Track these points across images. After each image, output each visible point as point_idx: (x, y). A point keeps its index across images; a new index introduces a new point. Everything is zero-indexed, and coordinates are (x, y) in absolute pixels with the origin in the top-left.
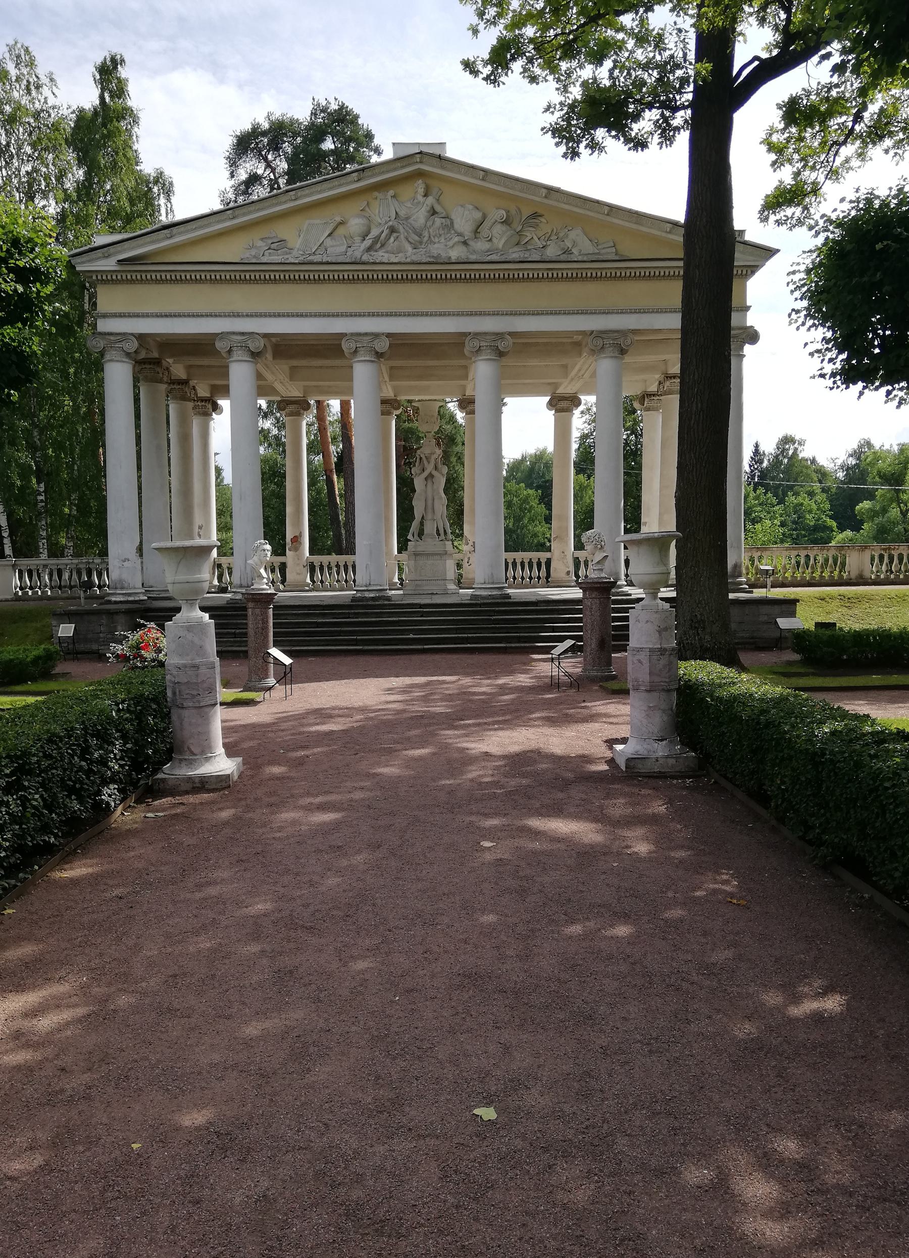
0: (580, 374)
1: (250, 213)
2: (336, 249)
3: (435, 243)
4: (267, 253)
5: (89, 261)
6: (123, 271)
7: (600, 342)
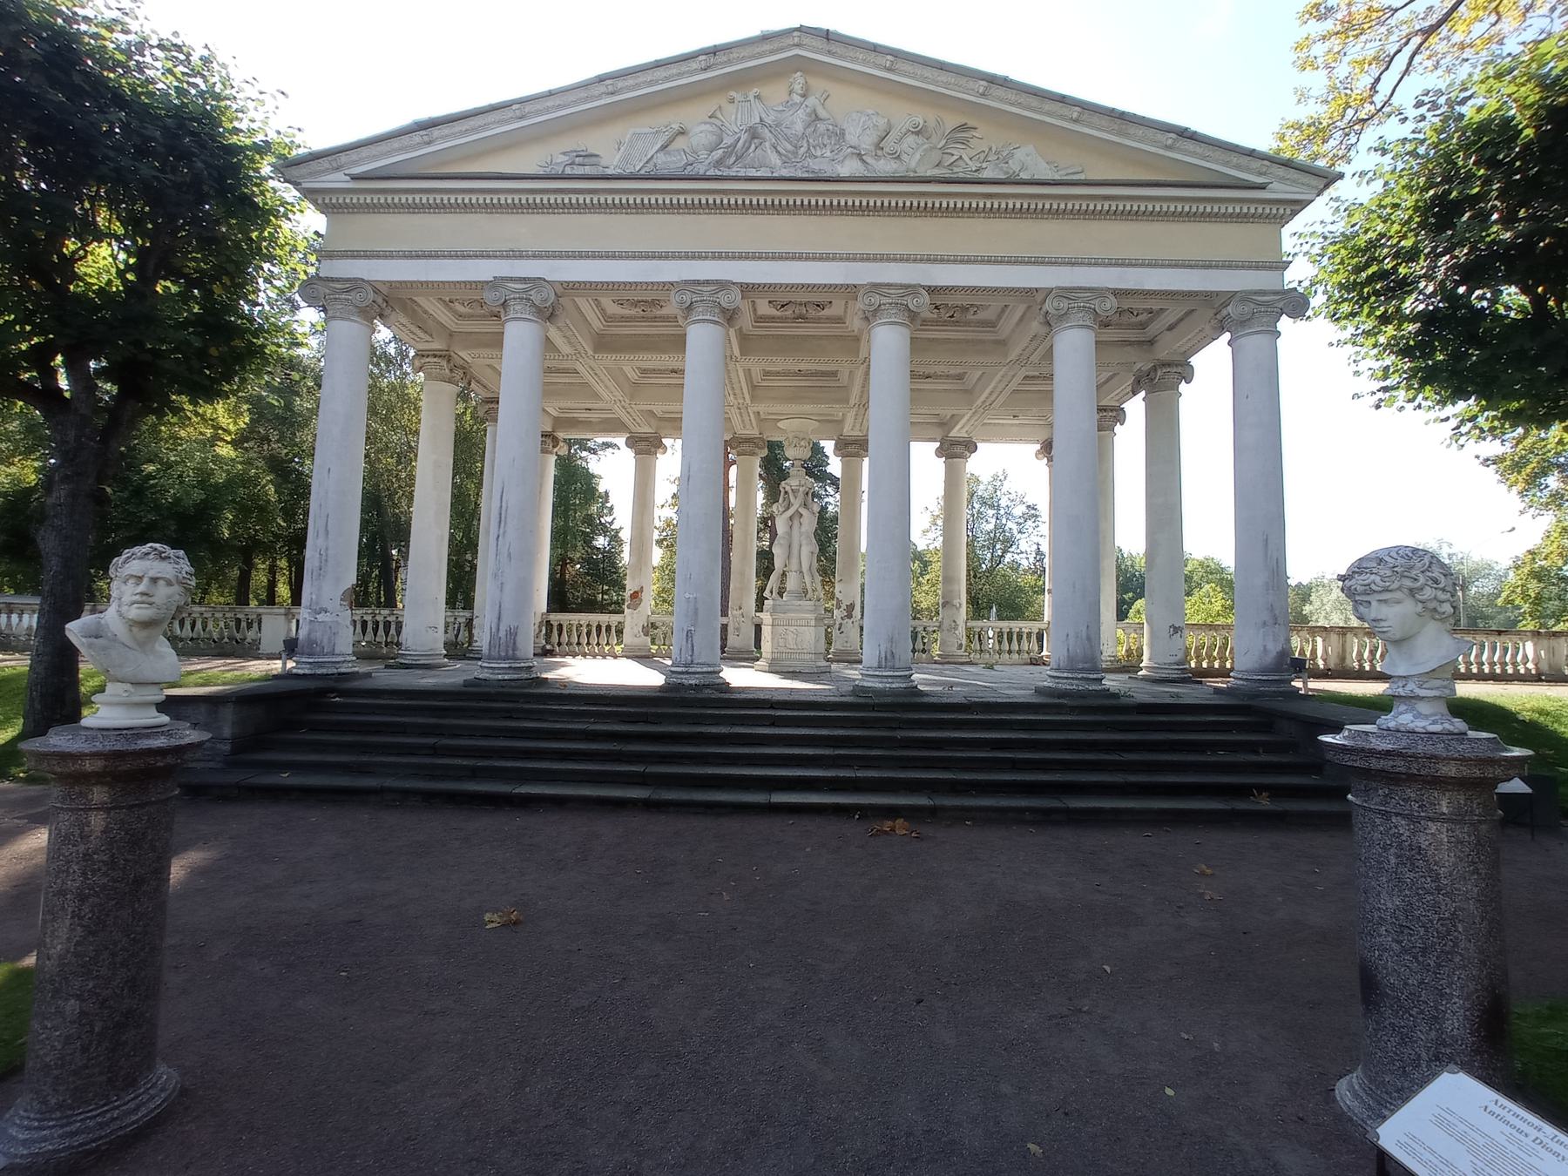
3: (816, 157)
5: (311, 174)
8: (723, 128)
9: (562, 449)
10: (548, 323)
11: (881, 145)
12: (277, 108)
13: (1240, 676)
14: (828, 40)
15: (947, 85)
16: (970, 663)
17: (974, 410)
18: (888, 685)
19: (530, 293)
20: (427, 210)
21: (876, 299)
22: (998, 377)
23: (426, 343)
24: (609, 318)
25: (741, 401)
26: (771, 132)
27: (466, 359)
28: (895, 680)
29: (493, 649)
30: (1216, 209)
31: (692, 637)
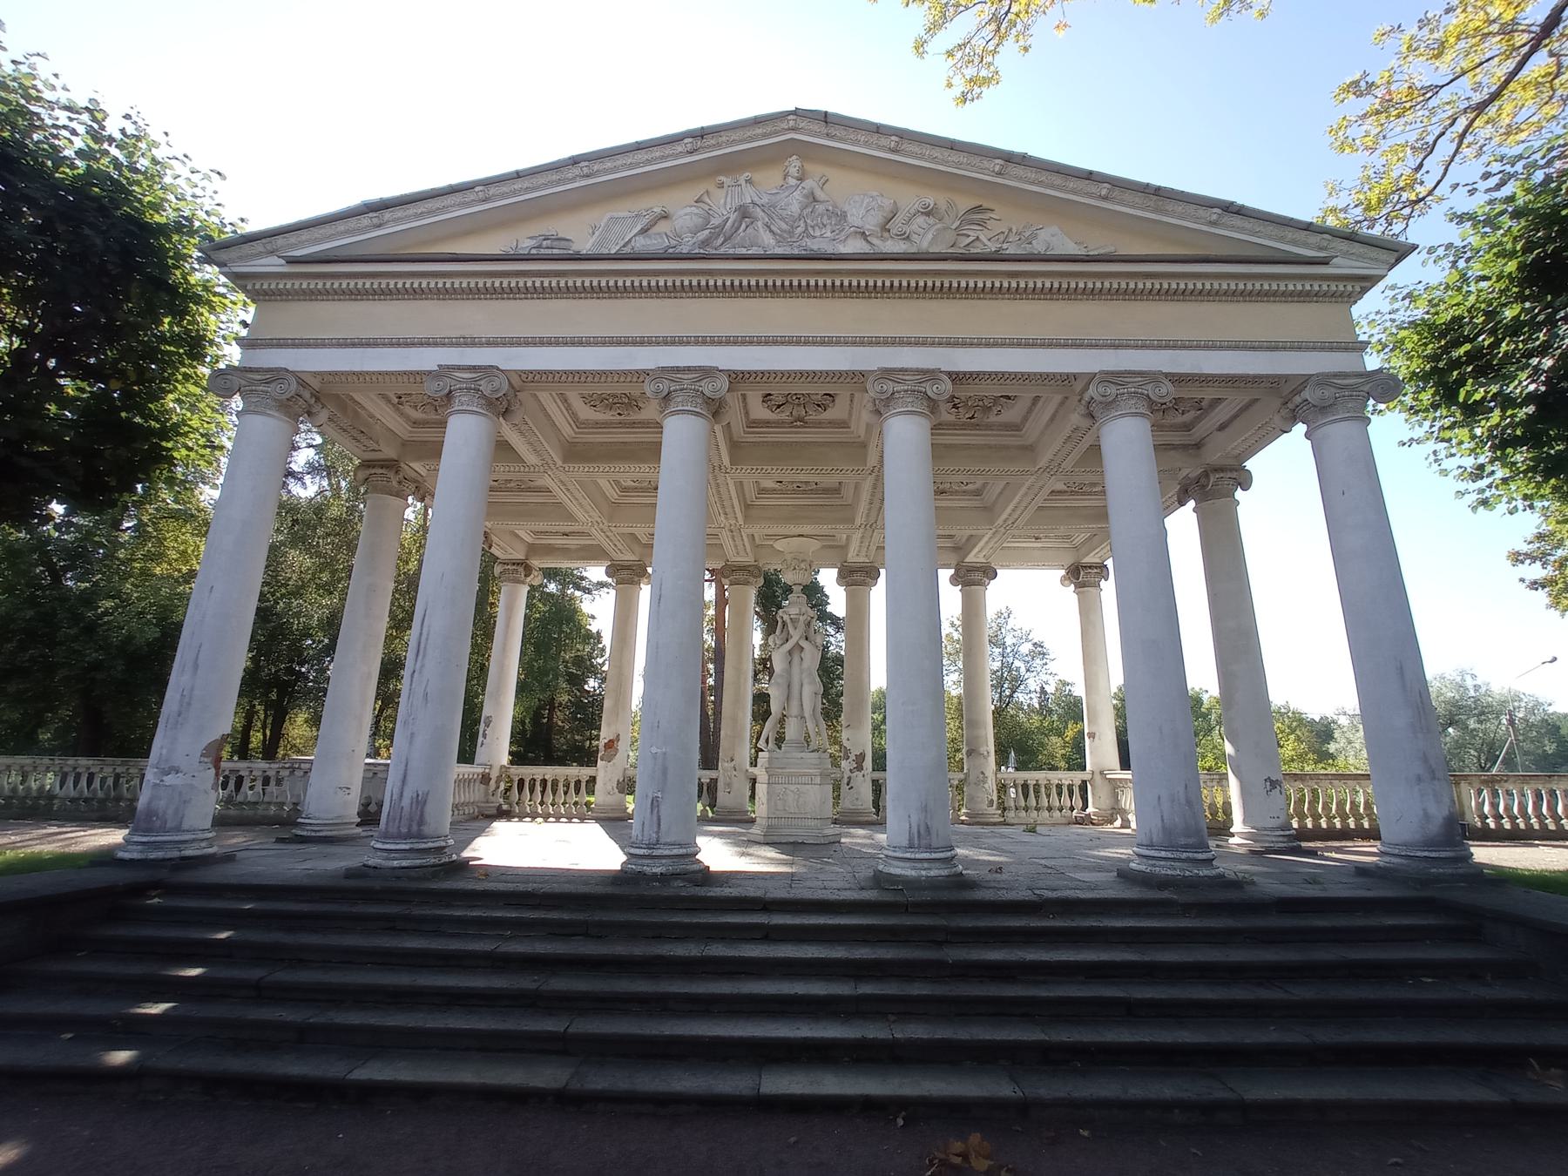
3: (815, 237)
5: (241, 258)
8: (711, 212)
9: (536, 579)
10: (501, 418)
11: (887, 227)
12: (216, 192)
13: (1396, 851)
14: (826, 122)
15: (958, 165)
16: (1005, 824)
17: (994, 530)
18: (924, 873)
19: (478, 383)
20: (371, 297)
21: (889, 387)
22: (1024, 489)
23: (373, 453)
24: (579, 424)
25: (733, 522)
26: (764, 211)
27: (419, 471)
28: (933, 865)
29: (391, 824)
30: (1274, 287)
31: (658, 806)
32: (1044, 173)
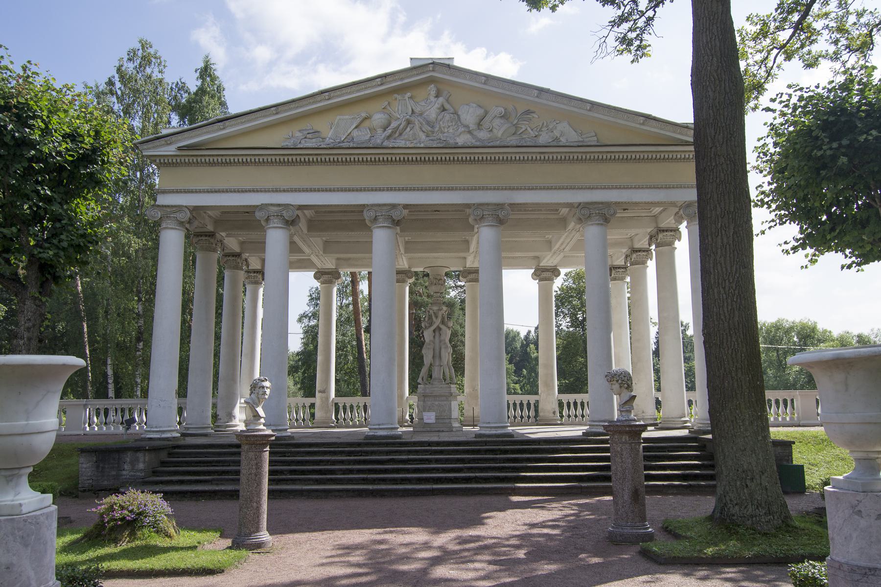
0: (562, 248)
1: (291, 109)
2: (362, 136)
4: (303, 142)
5: (154, 147)
6: (182, 156)
7: (586, 212)
32: (559, 97)
